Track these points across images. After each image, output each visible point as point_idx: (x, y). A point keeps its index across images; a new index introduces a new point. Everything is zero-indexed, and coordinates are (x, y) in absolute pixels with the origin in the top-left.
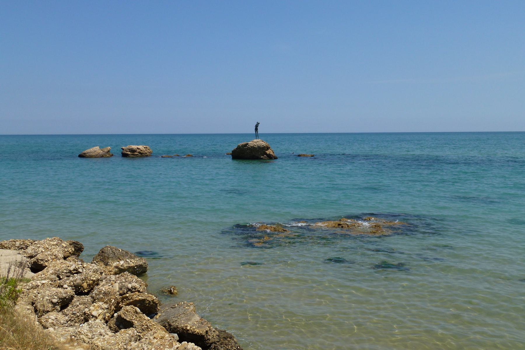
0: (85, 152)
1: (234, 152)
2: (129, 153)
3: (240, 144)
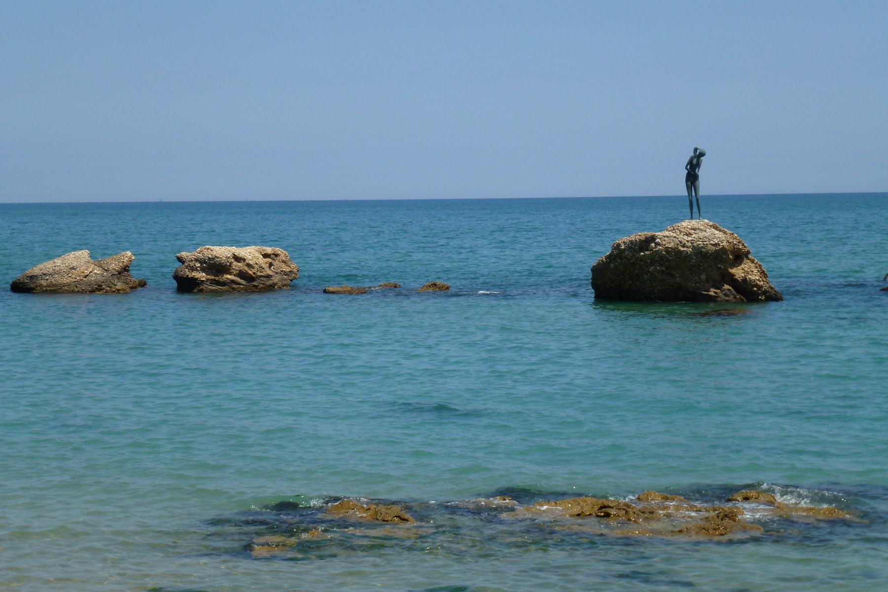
0: (36, 270)
1: (599, 271)
2: (201, 276)
3: (624, 239)
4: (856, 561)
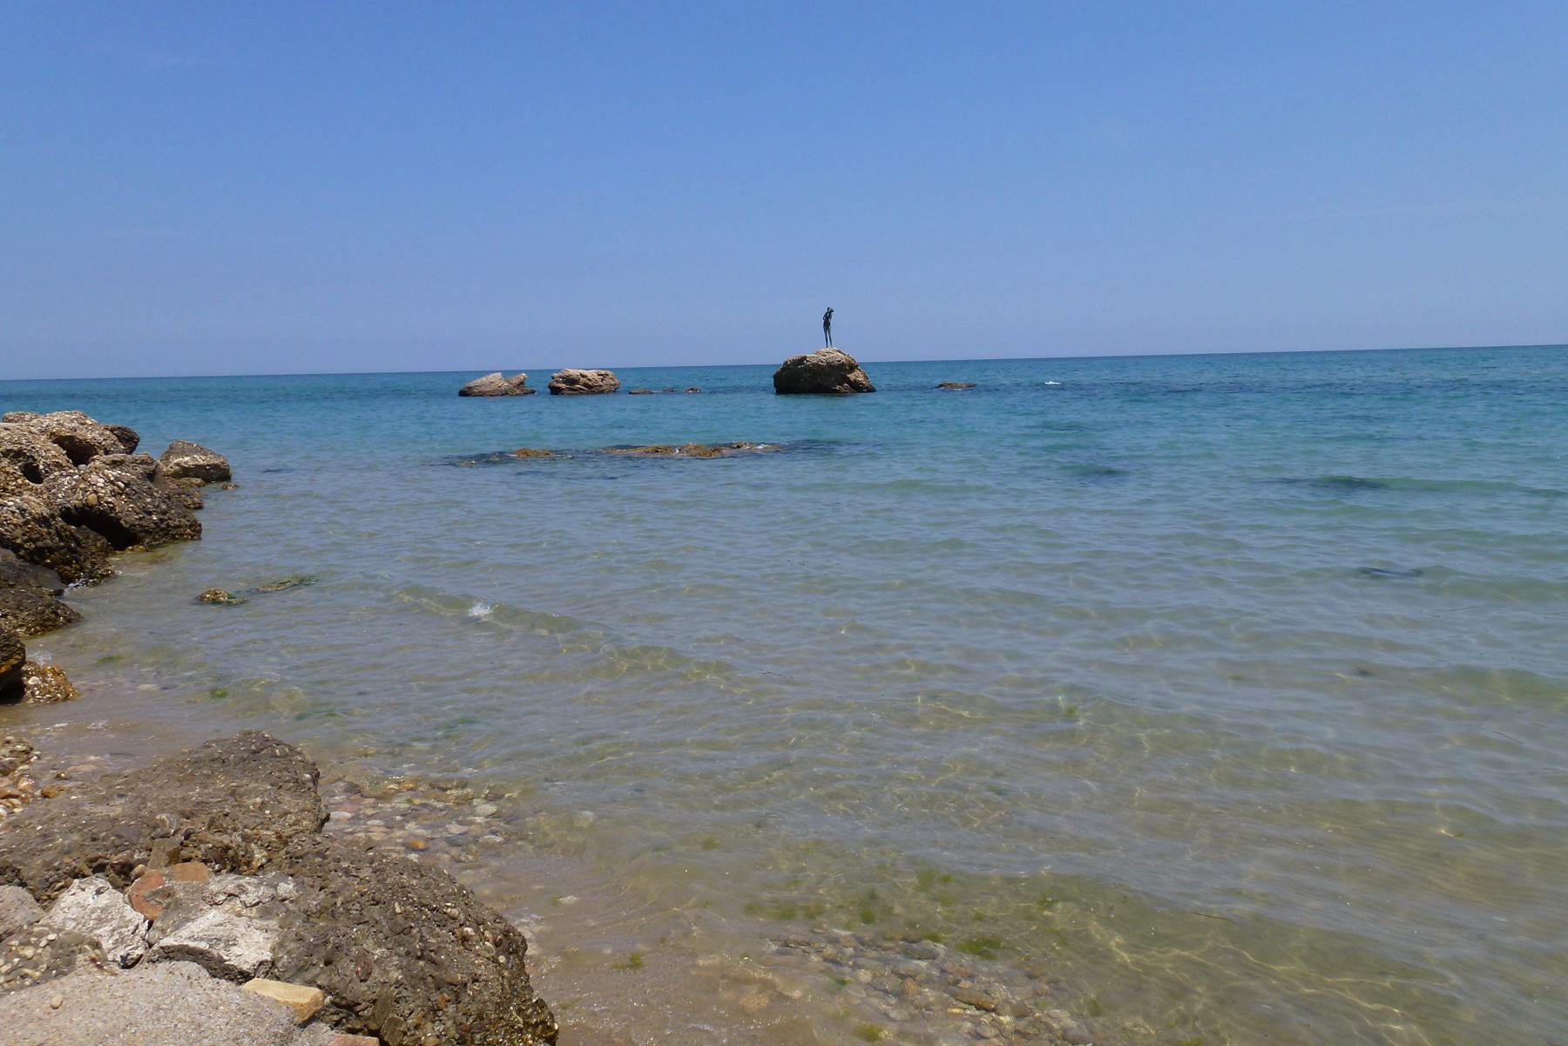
0: (472, 384)
1: (777, 377)
2: (563, 386)
4: (1495, 613)
